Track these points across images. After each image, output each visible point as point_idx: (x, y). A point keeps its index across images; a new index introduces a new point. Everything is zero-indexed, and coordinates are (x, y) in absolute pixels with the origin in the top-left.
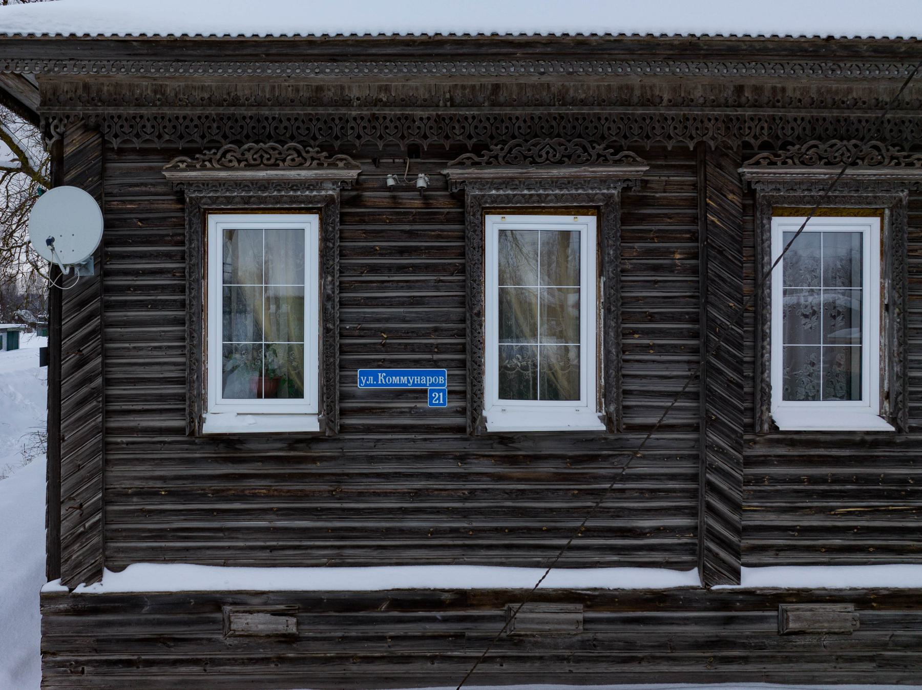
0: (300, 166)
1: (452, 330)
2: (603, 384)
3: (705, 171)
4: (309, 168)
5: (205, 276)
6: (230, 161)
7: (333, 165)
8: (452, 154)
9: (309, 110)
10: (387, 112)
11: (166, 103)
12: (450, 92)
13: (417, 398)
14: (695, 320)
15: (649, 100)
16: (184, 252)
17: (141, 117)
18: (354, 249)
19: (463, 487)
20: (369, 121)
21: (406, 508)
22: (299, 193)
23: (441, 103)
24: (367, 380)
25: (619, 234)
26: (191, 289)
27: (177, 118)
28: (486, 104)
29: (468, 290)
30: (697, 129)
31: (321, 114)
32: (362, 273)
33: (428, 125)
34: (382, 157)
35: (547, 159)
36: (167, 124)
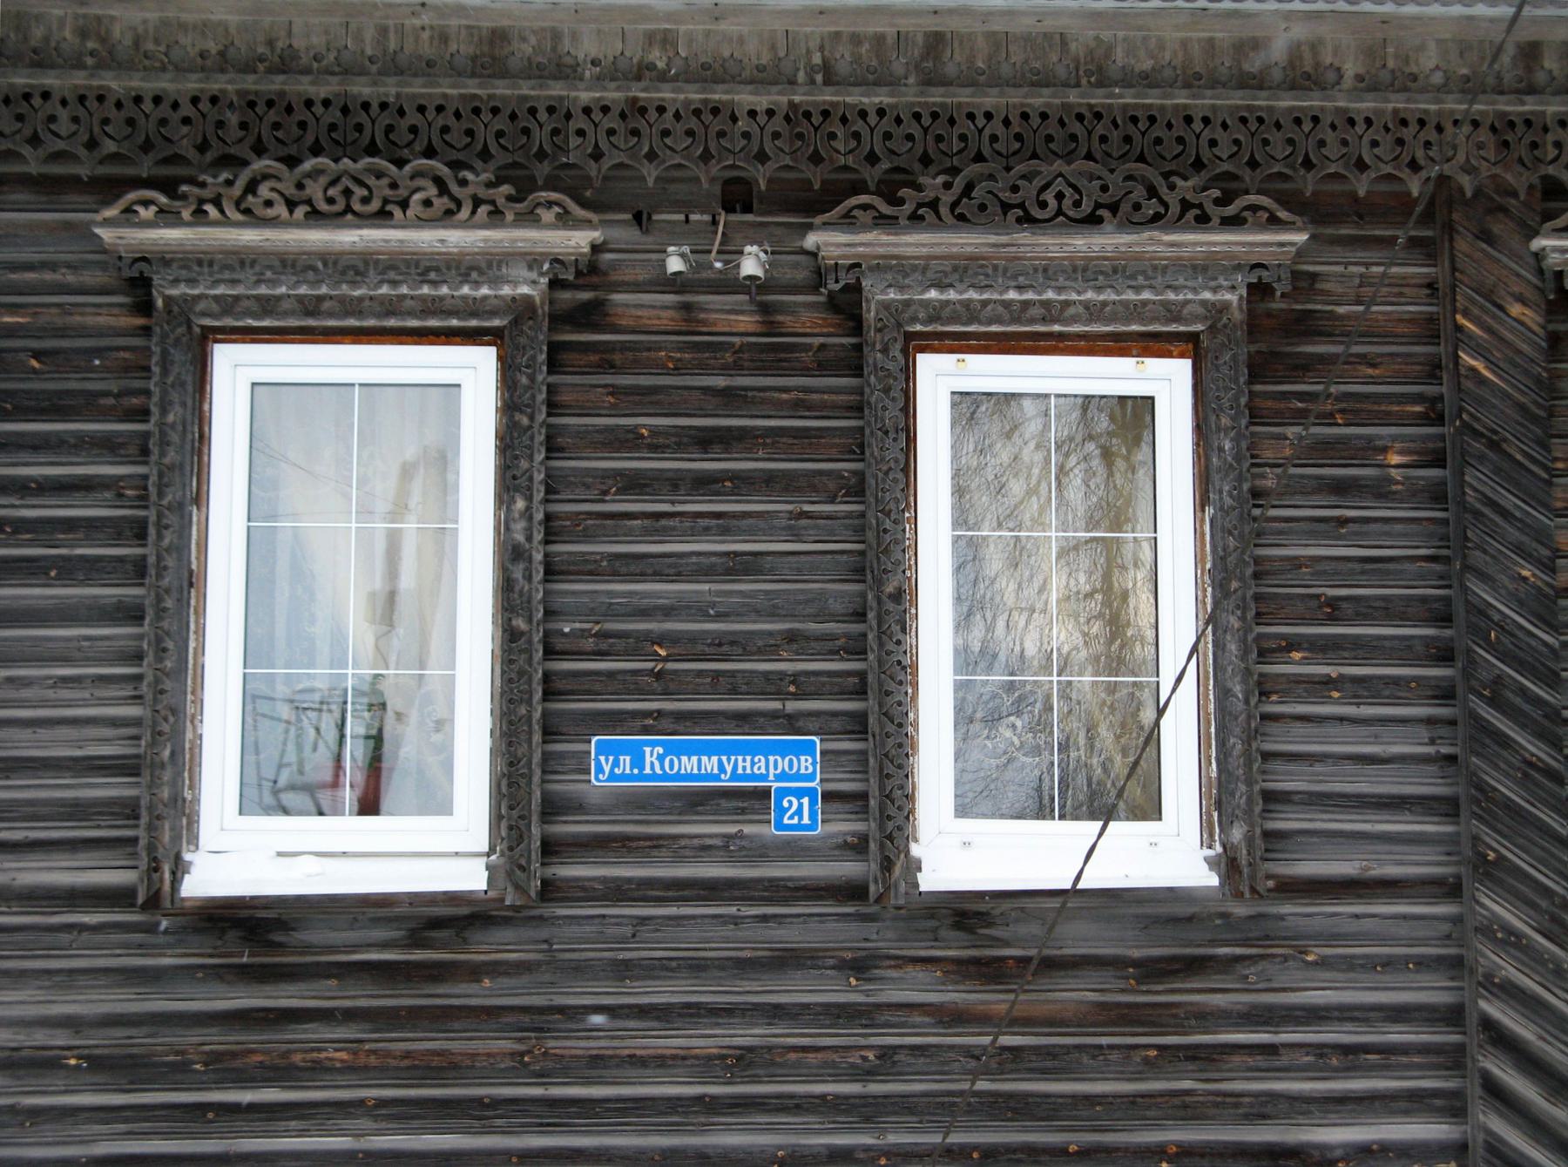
0: (448, 217)
1: (832, 637)
2: (1214, 775)
3: (1452, 248)
4: (464, 225)
5: (200, 498)
6: (269, 203)
7: (529, 218)
8: (814, 203)
9: (472, 87)
10: (666, 94)
11: (109, 59)
12: (821, 48)
13: (743, 811)
14: (1444, 618)
15: (1307, 76)
16: (146, 435)
17: (46, 95)
18: (582, 433)
19: (862, 1041)
20: (623, 116)
21: (713, 1097)
22: (444, 290)
23: (801, 77)
24: (616, 764)
25: (1243, 401)
26: (161, 527)
27: (138, 100)
28: (911, 80)
29: (870, 535)
30: (1428, 144)
31: (504, 98)
32: (605, 493)
33: (770, 129)
34: (657, 209)
35: (1060, 212)
36: (112, 113)
